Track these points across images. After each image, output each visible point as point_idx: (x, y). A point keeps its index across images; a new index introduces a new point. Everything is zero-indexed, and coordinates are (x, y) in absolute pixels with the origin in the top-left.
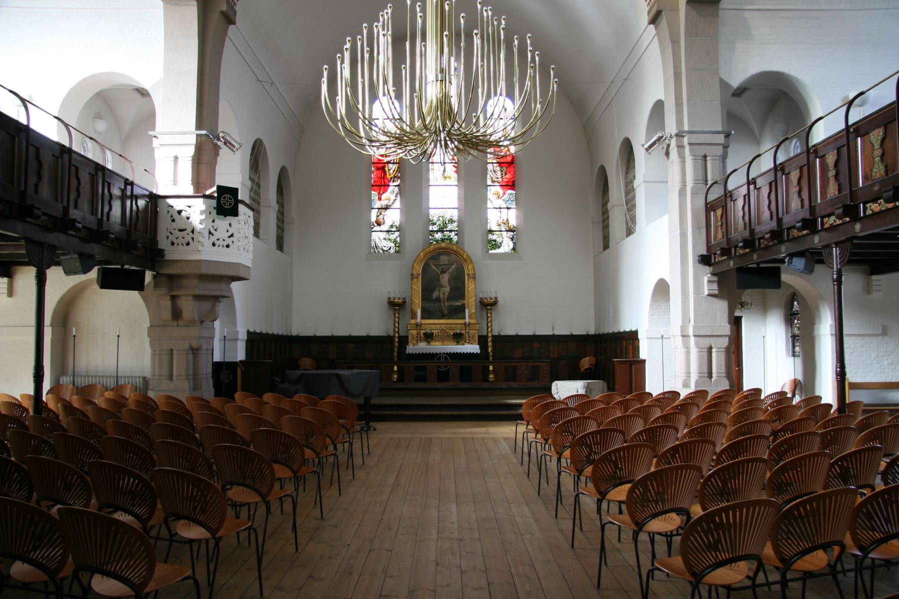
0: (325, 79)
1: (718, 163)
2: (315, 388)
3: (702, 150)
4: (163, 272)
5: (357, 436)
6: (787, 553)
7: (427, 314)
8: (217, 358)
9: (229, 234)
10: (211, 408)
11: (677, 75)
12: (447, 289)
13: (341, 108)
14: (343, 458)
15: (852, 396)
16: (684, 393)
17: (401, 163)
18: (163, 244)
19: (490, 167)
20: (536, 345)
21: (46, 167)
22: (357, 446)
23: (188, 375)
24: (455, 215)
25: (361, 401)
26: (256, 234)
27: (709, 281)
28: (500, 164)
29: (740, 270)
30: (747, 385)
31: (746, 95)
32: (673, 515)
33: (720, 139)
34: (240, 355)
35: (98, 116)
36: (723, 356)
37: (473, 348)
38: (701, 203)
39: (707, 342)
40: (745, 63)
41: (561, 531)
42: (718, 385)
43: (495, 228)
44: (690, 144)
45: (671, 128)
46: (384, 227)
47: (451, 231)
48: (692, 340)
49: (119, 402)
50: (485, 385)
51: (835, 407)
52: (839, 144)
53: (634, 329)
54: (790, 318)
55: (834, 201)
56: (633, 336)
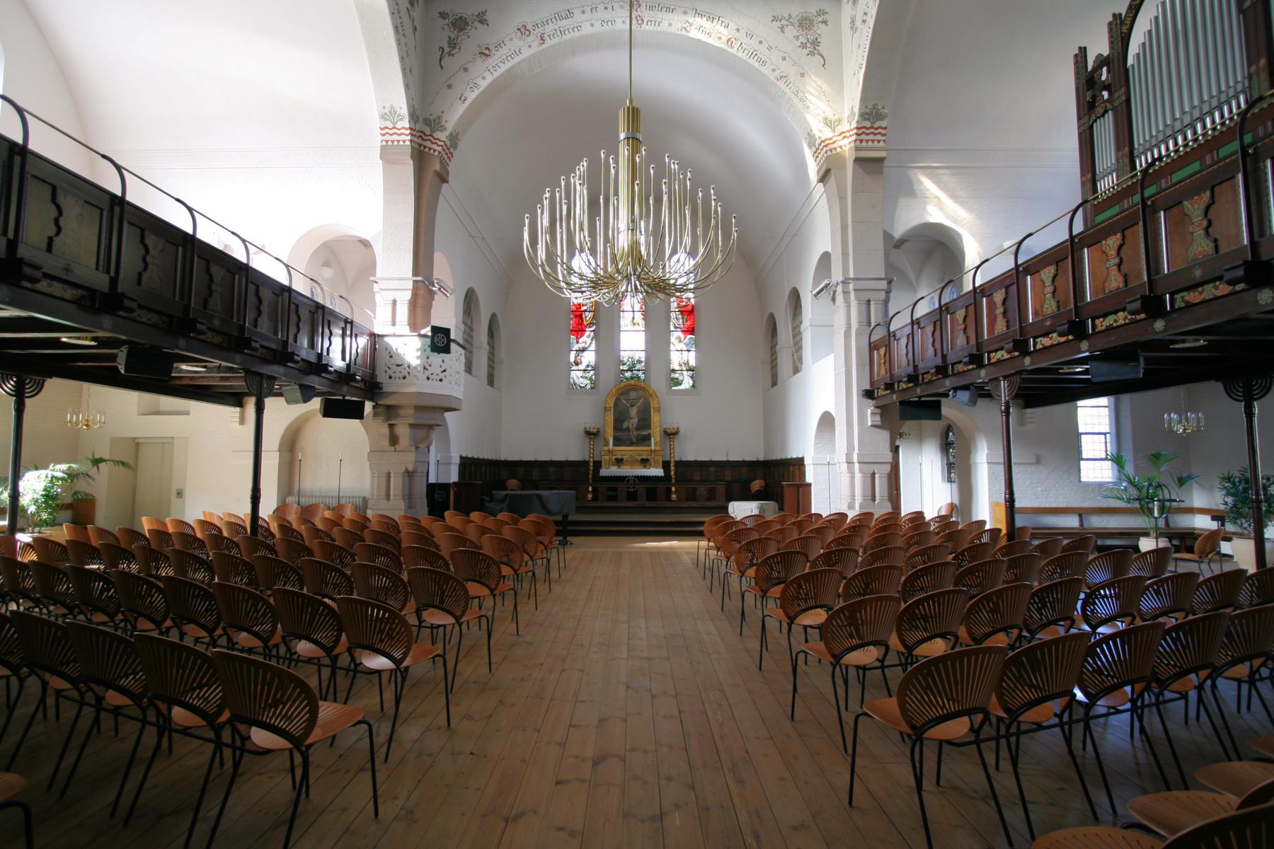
0: (526, 228)
1: (881, 306)
2: (518, 508)
3: (866, 296)
4: (381, 402)
5: (554, 553)
6: (910, 642)
7: (618, 441)
8: (432, 480)
10: (420, 528)
11: (844, 228)
12: (635, 421)
13: (542, 254)
14: (540, 572)
15: (1020, 521)
16: (851, 515)
17: (597, 307)
18: (382, 378)
19: (673, 315)
20: (712, 469)
21: (265, 303)
22: (554, 560)
23: (403, 496)
24: (642, 356)
25: (559, 518)
26: (469, 369)
27: (872, 414)
28: (682, 312)
29: (902, 403)
30: (906, 509)
31: (905, 247)
32: (871, 648)
33: (884, 285)
34: (454, 477)
35: (327, 264)
36: (885, 481)
37: (658, 472)
39: (870, 468)
41: (747, 650)
42: (881, 509)
43: (677, 367)
45: (837, 275)
46: (582, 367)
48: (857, 466)
49: (335, 523)
50: (669, 504)
51: (1004, 531)
52: (1007, 283)
54: (946, 447)
55: (1002, 337)
56: (800, 462)
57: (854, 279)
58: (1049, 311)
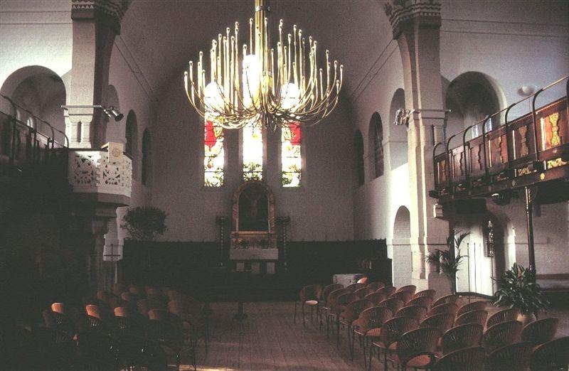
9: (117, 175)
38: (431, 156)
40: (456, 66)
44: (422, 118)
45: (410, 106)
46: (214, 169)
47: (258, 172)
48: (426, 247)
53: (383, 239)
56: (294, 143)
57: (421, 110)
58: (556, 144)
